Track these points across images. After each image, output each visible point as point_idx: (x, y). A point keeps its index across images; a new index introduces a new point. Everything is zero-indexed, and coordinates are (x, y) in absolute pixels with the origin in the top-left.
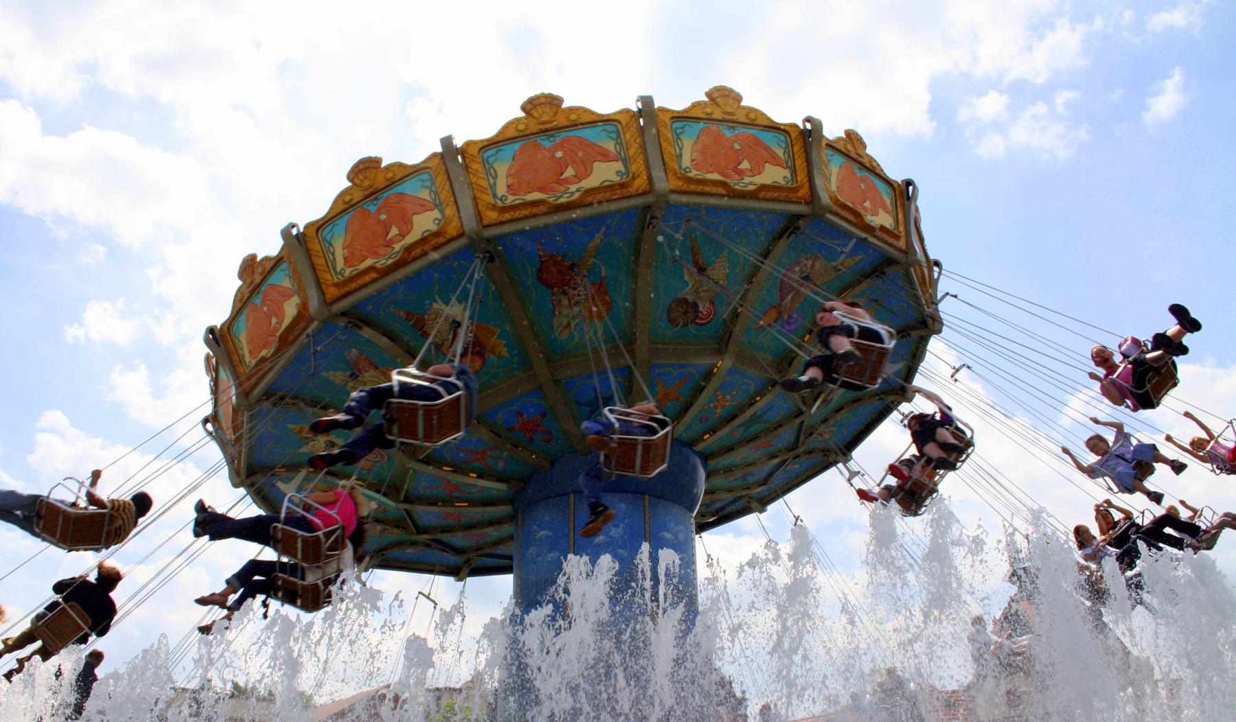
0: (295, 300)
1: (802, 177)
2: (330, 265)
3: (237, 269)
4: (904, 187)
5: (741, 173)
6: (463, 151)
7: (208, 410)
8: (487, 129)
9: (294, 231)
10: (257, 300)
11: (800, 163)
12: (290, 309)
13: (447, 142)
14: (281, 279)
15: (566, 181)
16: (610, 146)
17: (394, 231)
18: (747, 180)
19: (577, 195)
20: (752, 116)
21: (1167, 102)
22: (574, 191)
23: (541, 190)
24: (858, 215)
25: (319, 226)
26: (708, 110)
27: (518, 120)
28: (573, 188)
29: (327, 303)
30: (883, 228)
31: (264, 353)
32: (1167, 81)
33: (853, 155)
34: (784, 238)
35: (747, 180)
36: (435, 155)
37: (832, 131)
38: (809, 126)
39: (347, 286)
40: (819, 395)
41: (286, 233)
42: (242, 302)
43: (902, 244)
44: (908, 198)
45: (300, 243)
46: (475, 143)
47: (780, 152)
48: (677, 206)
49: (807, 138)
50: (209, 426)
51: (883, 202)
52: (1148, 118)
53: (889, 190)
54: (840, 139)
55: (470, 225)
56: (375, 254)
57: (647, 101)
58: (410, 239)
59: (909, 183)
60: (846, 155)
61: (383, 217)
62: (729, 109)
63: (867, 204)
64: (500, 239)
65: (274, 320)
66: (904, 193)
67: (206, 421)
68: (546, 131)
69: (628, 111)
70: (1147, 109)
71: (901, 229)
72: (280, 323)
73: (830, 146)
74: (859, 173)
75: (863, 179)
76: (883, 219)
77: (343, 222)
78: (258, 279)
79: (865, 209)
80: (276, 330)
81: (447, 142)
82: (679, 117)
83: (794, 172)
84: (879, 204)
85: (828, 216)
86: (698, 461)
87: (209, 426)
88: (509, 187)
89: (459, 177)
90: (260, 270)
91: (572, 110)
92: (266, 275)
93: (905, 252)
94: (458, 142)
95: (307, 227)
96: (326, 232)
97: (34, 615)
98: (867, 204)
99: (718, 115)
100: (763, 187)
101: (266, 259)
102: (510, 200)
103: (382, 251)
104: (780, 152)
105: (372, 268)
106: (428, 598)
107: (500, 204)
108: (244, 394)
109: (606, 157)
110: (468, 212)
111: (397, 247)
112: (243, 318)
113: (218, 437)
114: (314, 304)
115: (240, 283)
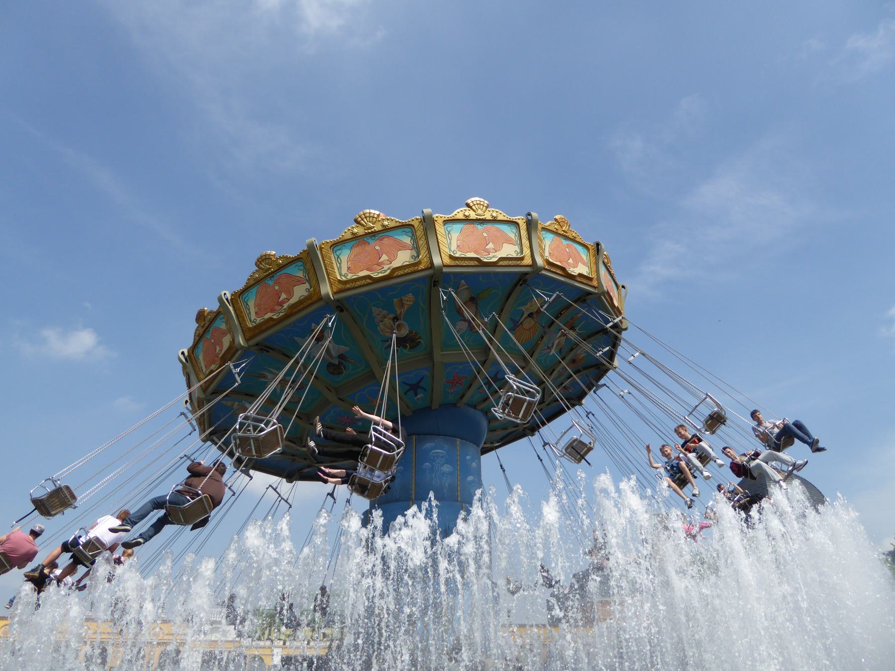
1: (527, 251)
10: (208, 336)
11: (525, 242)
15: (382, 263)
17: (283, 296)
18: (491, 255)
19: (388, 272)
22: (386, 270)
24: (563, 269)
30: (580, 275)
34: (518, 286)
36: (304, 251)
40: (294, 443)
42: (199, 338)
47: (512, 236)
48: (448, 274)
51: (581, 258)
56: (272, 311)
58: (293, 300)
61: (277, 288)
63: (571, 261)
65: (218, 348)
72: (221, 350)
77: (254, 290)
80: (218, 354)
84: (578, 260)
85: (543, 272)
86: (472, 410)
88: (348, 268)
92: (212, 321)
97: (221, 505)
100: (501, 259)
101: (211, 312)
102: (350, 276)
103: (277, 308)
106: (275, 490)
107: (344, 279)
111: (285, 306)
112: (200, 345)
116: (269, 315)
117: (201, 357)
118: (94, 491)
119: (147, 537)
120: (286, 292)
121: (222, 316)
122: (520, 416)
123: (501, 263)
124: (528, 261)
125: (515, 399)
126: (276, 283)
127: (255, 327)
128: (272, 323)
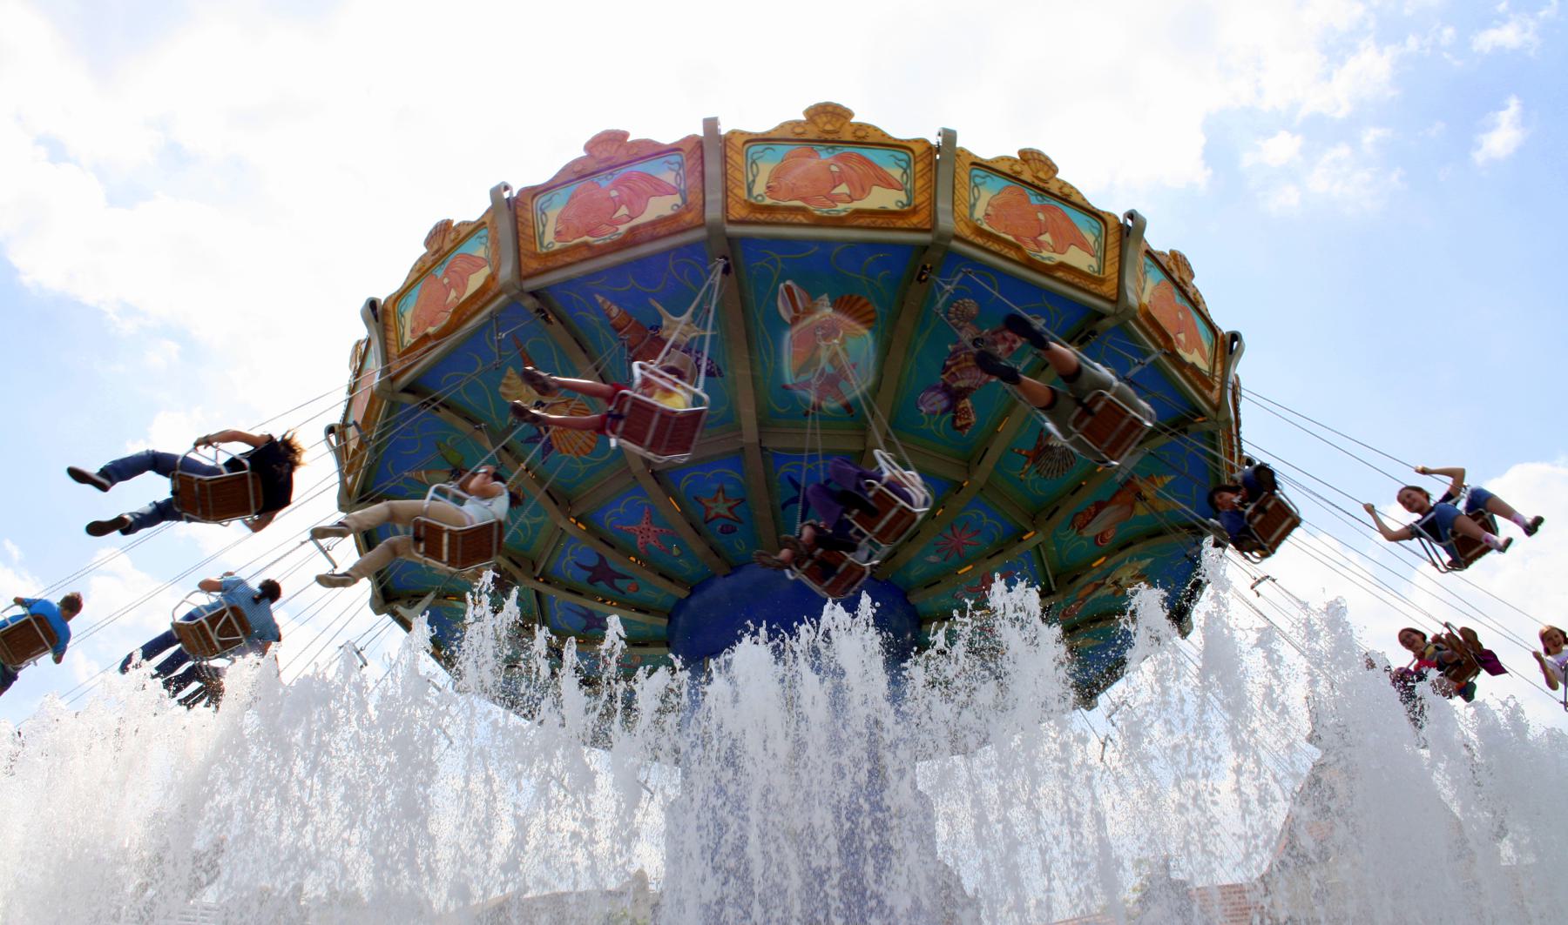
0: (486, 271)
1: (1111, 271)
2: (537, 237)
3: (425, 235)
4: (1228, 339)
5: (1040, 245)
6: (726, 141)
7: (336, 418)
8: (762, 122)
9: (506, 195)
10: (440, 273)
11: (1113, 254)
12: (475, 282)
13: (711, 124)
14: (477, 248)
16: (896, 173)
17: (623, 211)
20: (1066, 190)
21: (1502, 138)
23: (803, 199)
25: (533, 192)
26: (1017, 168)
27: (798, 123)
28: (841, 206)
29: (522, 274)
30: (1193, 366)
31: (431, 330)
32: (1502, 113)
33: (1176, 276)
35: (1045, 254)
37: (1157, 239)
38: (1129, 223)
39: (552, 260)
41: (496, 193)
43: (1214, 396)
44: (1231, 351)
45: (513, 211)
46: (743, 133)
47: (1091, 239)
49: (1128, 232)
50: (333, 438)
52: (1479, 157)
53: (1210, 335)
54: (1163, 254)
55: (713, 213)
57: (949, 136)
59: (1235, 337)
60: (1167, 273)
62: (1041, 175)
64: (747, 240)
66: (1228, 346)
67: (331, 430)
68: (826, 141)
69: (925, 141)
70: (1479, 147)
71: (1218, 373)
73: (1150, 254)
74: (1178, 299)
75: (1183, 309)
76: (1197, 358)
78: (448, 245)
79: (1179, 341)
81: (711, 124)
82: (978, 164)
83: (1103, 261)
84: (1195, 343)
87: (333, 438)
89: (713, 168)
90: (453, 236)
91: (861, 126)
92: (459, 242)
93: (1217, 408)
94: (724, 130)
95: (524, 191)
96: (541, 200)
98: (1182, 337)
99: (1027, 177)
104: (1091, 239)
105: (586, 245)
108: (390, 379)
109: (888, 183)
110: (714, 196)
112: (415, 292)
113: (340, 453)
114: (506, 272)
115: (425, 250)
116: (587, 238)
117: (408, 315)
118: (256, 498)
119: (124, 526)
120: (629, 204)
121: (483, 232)
122: (893, 512)
123: (1059, 274)
124: (1109, 289)
125: (880, 493)
126: (616, 186)
127: (547, 255)
128: (586, 253)
